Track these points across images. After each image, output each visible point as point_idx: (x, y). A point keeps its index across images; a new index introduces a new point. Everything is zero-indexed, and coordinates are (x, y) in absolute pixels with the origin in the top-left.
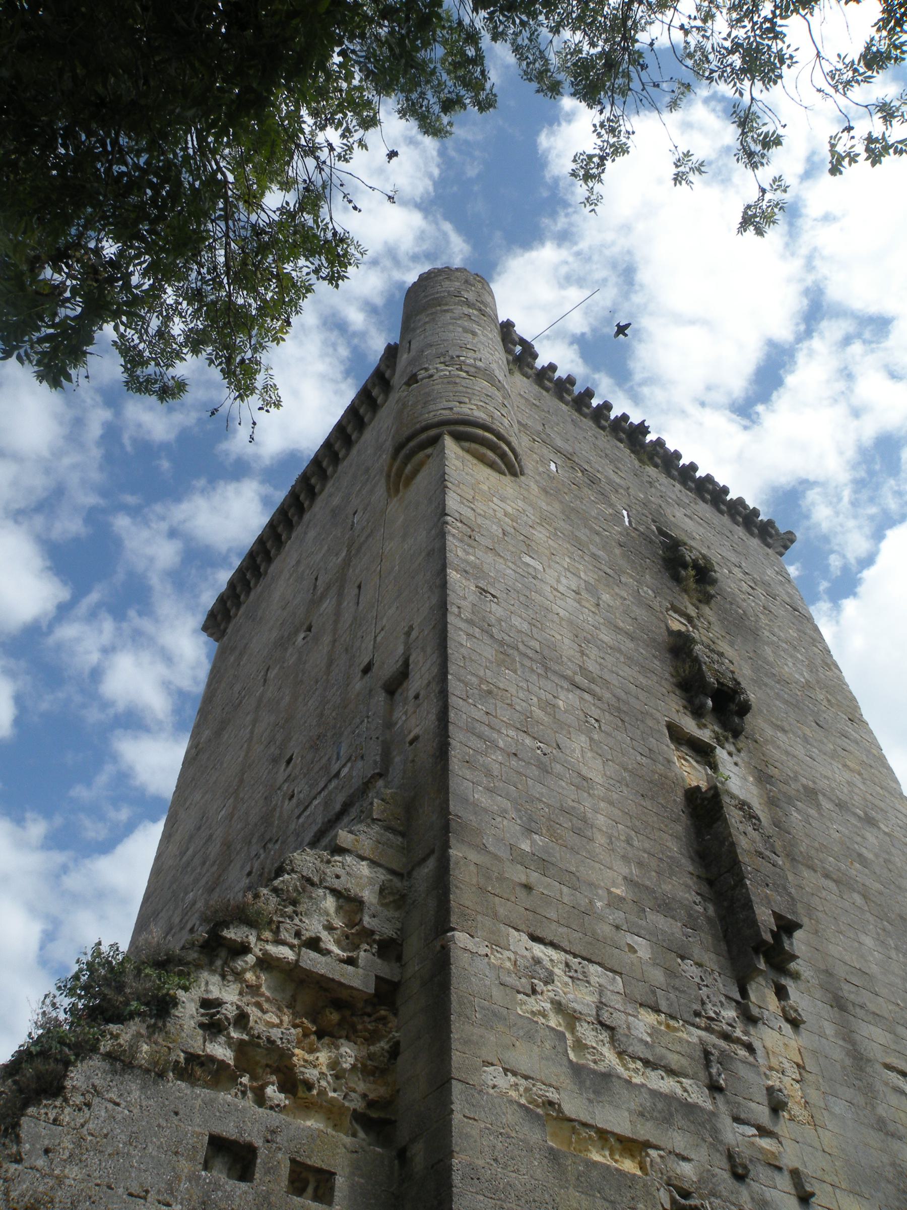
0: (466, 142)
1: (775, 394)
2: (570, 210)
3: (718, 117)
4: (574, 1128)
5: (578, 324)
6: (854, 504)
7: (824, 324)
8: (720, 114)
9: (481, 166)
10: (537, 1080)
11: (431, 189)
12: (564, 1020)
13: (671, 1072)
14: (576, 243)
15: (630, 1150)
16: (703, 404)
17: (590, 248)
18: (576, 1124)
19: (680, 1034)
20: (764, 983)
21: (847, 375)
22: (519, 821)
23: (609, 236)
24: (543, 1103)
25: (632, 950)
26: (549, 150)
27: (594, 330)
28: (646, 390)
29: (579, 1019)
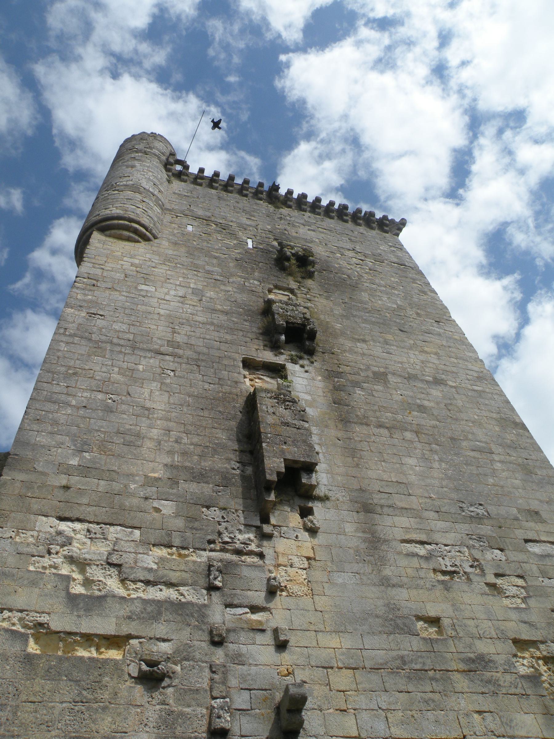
0: (234, 102)
1: (467, 180)
2: (308, 119)
3: (377, 31)
4: (60, 637)
5: (337, 180)
6: (537, 227)
7: (482, 128)
8: (377, 29)
9: (249, 113)
10: (31, 611)
11: (225, 135)
12: (77, 567)
13: (170, 585)
14: (318, 136)
15: (117, 643)
16: (426, 200)
17: (328, 134)
18: (62, 635)
19: (190, 558)
20: (289, 510)
21: (508, 152)
22: (73, 447)
23: (336, 125)
24: (35, 625)
25: (157, 510)
26: (283, 88)
27: (347, 181)
28: (390, 203)
29: (89, 565)
